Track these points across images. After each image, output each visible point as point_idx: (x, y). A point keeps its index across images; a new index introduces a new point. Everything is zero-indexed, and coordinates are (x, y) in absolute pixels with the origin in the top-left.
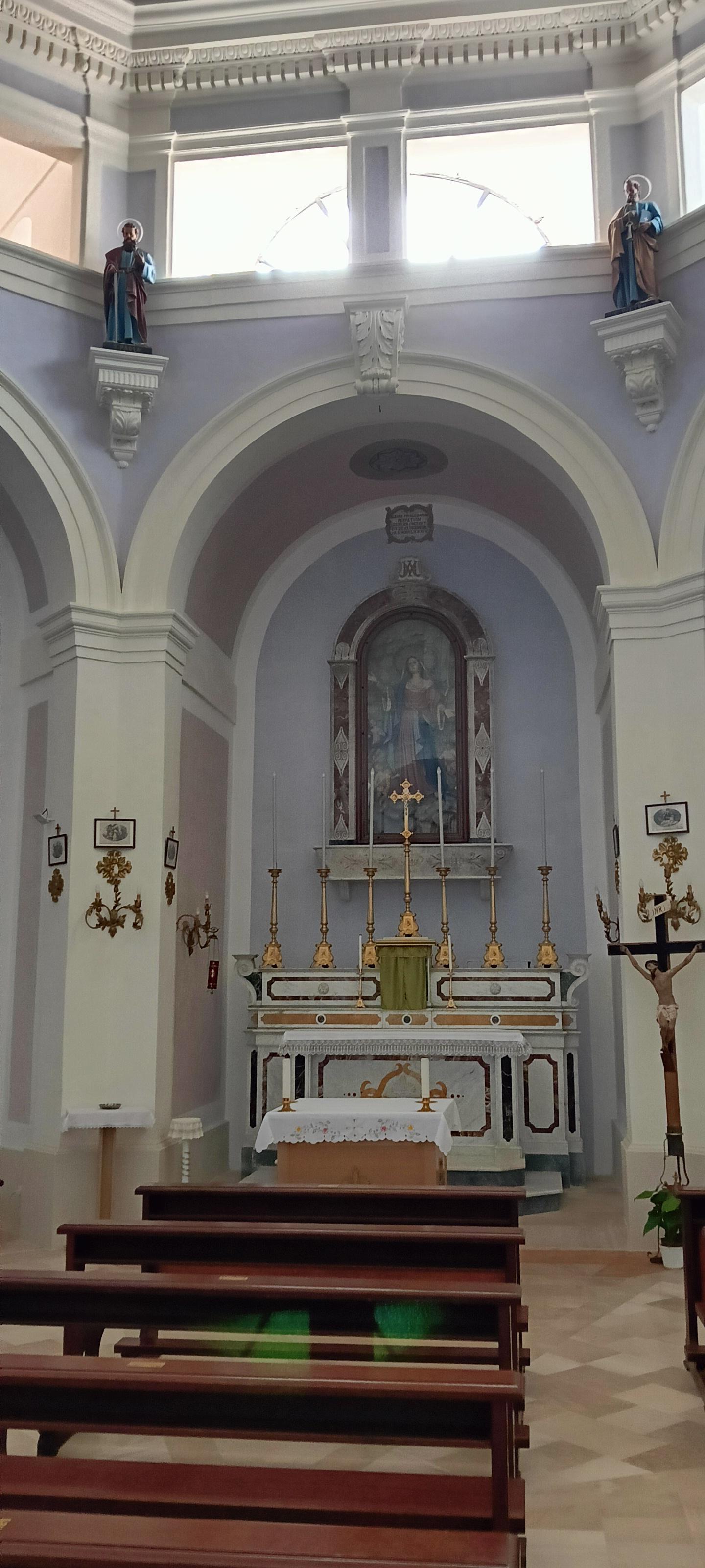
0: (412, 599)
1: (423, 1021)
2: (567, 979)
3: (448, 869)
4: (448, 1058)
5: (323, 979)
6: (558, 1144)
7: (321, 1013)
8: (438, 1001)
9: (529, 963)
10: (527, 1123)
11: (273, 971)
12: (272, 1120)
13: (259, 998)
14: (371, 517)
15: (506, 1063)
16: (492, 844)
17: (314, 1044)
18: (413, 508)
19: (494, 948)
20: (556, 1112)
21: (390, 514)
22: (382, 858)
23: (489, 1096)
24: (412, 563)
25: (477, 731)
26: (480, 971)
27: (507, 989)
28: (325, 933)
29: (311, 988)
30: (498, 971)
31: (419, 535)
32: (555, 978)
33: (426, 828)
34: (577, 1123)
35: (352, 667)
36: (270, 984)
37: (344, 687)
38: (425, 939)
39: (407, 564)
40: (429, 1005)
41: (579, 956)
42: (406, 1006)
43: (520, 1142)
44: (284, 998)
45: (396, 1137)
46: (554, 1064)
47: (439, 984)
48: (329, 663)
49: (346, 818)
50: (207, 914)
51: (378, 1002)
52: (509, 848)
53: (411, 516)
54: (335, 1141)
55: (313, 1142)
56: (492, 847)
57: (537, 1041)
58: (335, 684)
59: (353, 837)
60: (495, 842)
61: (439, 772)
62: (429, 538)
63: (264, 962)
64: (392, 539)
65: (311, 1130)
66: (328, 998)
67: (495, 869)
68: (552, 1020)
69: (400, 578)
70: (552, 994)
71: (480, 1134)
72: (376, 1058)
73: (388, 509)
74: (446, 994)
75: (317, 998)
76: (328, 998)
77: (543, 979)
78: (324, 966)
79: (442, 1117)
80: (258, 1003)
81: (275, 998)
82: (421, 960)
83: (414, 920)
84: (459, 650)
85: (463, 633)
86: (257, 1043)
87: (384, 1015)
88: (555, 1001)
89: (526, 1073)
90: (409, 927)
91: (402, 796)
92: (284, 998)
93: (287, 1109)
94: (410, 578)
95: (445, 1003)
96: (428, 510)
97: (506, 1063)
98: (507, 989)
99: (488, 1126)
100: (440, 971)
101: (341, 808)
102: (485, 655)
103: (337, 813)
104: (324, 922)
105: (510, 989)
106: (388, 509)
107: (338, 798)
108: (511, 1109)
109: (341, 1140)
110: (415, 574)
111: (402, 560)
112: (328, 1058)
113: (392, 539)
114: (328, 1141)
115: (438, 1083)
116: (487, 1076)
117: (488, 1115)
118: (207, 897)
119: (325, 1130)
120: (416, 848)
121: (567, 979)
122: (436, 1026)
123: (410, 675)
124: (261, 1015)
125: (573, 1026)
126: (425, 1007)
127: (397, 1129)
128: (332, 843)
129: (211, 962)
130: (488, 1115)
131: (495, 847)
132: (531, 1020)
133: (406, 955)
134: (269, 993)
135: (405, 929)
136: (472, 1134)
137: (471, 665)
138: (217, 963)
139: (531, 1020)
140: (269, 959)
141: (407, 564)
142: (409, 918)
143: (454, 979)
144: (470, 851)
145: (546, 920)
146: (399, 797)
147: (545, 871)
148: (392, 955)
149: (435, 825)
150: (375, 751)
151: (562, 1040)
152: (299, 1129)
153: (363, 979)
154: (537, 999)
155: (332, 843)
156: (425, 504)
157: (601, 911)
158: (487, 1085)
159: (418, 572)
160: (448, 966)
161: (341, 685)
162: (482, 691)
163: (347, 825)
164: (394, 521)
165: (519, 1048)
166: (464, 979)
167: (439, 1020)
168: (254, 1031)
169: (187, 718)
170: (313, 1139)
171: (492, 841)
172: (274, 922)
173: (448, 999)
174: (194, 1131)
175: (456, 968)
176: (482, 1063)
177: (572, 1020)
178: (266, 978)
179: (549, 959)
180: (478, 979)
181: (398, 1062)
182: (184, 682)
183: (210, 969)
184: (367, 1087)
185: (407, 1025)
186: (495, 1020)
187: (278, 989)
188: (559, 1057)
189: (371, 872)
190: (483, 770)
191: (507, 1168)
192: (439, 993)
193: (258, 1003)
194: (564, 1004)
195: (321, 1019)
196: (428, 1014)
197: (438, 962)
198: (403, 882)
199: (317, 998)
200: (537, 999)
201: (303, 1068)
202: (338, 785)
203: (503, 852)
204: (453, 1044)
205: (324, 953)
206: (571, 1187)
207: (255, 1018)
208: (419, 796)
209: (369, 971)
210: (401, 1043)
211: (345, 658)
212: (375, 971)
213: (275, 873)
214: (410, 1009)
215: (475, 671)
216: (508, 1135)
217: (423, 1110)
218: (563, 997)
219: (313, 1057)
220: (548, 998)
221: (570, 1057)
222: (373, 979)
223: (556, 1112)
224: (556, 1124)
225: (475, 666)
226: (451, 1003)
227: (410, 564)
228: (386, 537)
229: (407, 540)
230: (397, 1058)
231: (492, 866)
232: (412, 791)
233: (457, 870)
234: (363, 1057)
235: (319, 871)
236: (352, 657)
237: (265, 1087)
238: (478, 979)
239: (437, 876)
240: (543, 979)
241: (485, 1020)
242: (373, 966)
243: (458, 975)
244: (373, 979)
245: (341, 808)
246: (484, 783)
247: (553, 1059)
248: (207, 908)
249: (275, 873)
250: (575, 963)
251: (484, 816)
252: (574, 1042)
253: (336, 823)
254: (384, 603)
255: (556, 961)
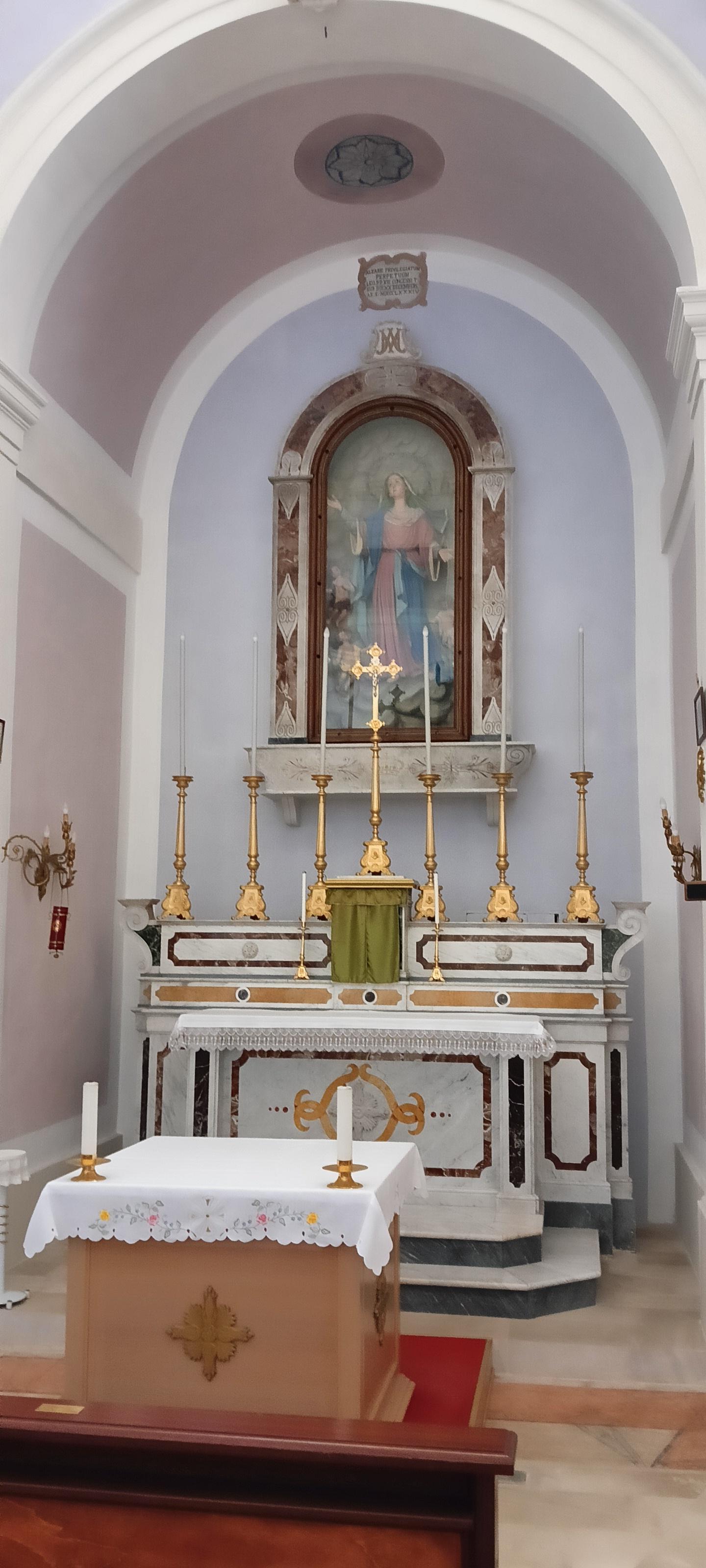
0: (397, 386)
1: (394, 999)
2: (612, 939)
3: (436, 778)
4: (427, 1058)
5: (249, 936)
6: (594, 1187)
7: (243, 986)
8: (417, 969)
9: (556, 916)
10: (549, 1155)
11: (177, 924)
12: (59, 1198)
13: (156, 962)
14: (334, 272)
15: (516, 1066)
16: (503, 743)
17: (224, 1034)
18: (398, 258)
19: (503, 892)
20: (593, 1138)
21: (365, 267)
22: (342, 763)
23: (489, 1116)
24: (394, 333)
25: (485, 578)
26: (481, 926)
27: (521, 953)
28: (254, 869)
29: (232, 949)
30: (509, 926)
31: (406, 297)
32: (595, 938)
33: (410, 723)
34: (625, 1155)
35: (305, 487)
36: (172, 942)
37: (293, 516)
38: (399, 878)
39: (387, 333)
40: (404, 975)
41: (632, 906)
42: (368, 976)
43: (538, 1186)
44: (191, 963)
45: (287, 1235)
46: (590, 1066)
47: (420, 945)
48: (272, 481)
49: (293, 706)
50: (66, 837)
51: (327, 971)
52: (530, 748)
53: (395, 270)
54: (171, 1239)
55: (131, 1241)
56: (503, 748)
57: (564, 1032)
58: (280, 512)
59: (302, 734)
60: (509, 739)
61: (425, 633)
62: (421, 301)
63: (165, 910)
64: (366, 305)
65: (128, 1217)
66: (257, 964)
67: (508, 777)
68: (590, 1001)
69: (376, 356)
70: (590, 961)
71: (474, 1174)
72: (319, 1055)
73: (362, 261)
74: (430, 960)
75: (240, 964)
76: (257, 964)
77: (575, 939)
78: (252, 918)
79: (373, 1201)
80: (155, 970)
81: (178, 963)
82: (392, 910)
83: (385, 851)
84: (462, 458)
85: (468, 434)
86: (149, 1028)
87: (336, 990)
88: (595, 972)
89: (547, 1079)
90: (376, 861)
91: (370, 669)
92: (191, 963)
93: (89, 1175)
94: (391, 355)
95: (426, 973)
96: (420, 263)
97: (516, 1066)
98: (521, 953)
99: (486, 1162)
100: (423, 926)
101: (285, 692)
102: (499, 465)
103: (280, 699)
104: (253, 853)
105: (526, 954)
106: (362, 261)
107: (283, 677)
108: (522, 1137)
109: (182, 1238)
110: (399, 350)
111: (381, 328)
112: (246, 1055)
113: (366, 305)
114: (158, 1238)
115: (411, 1095)
116: (487, 1084)
117: (487, 1144)
118: (66, 811)
119: (153, 1218)
120: (392, 752)
121: (612, 939)
122: (412, 1006)
123: (390, 500)
124: (155, 987)
125: (621, 1009)
126: (395, 978)
127: (287, 1219)
128: (272, 741)
129: (56, 908)
130: (487, 1144)
131: (508, 747)
132: (558, 1000)
133: (370, 902)
134: (171, 956)
135: (370, 864)
136: (462, 1173)
137: (479, 482)
138: (65, 910)
139: (558, 1000)
140: (171, 905)
141: (387, 334)
142: (376, 847)
143: (442, 938)
144: (471, 752)
145: (582, 852)
146: (365, 669)
147: (583, 778)
148: (350, 903)
149: (417, 713)
150: (340, 612)
151: (604, 1030)
152: (105, 1216)
153: (309, 937)
154: (566, 968)
155: (272, 741)
156: (416, 253)
157: (668, 834)
158: (487, 1098)
159: (402, 347)
160: (432, 919)
161: (289, 513)
162: (495, 520)
163: (295, 718)
164: (370, 278)
165: (535, 1046)
166: (458, 938)
167: (416, 998)
168: (144, 1010)
169: (32, 539)
170: (130, 1235)
171: (503, 738)
172: (180, 853)
173: (431, 966)
174: (12, 1173)
175: (446, 921)
176: (479, 1065)
177: (619, 1001)
178: (167, 934)
179: (586, 909)
180: (478, 938)
181: (352, 1061)
182: (19, 475)
183: (54, 919)
184: (304, 1098)
185: (370, 1005)
186: (502, 999)
187: (183, 950)
188: (598, 1056)
189: (324, 780)
190: (493, 635)
191: (512, 1235)
192: (420, 958)
193: (155, 970)
194: (608, 976)
195: (243, 995)
196: (400, 988)
197: (418, 912)
198: (368, 797)
199: (240, 964)
200: (566, 968)
201: (207, 1069)
202: (282, 659)
203: (519, 755)
204: (435, 1037)
205: (251, 899)
206: (614, 1250)
207: (148, 992)
208: (394, 669)
209: (316, 925)
210: (354, 1035)
211: (295, 473)
212: (326, 925)
213: (183, 781)
214: (374, 981)
215: (485, 488)
216: (517, 1177)
217: (338, 1184)
218: (607, 965)
219: (223, 1053)
220: (583, 968)
221: (615, 1057)
222: (323, 937)
223: (593, 1138)
224: (592, 1156)
225: (484, 482)
226: (437, 973)
227: (390, 334)
228: (359, 301)
229: (388, 305)
230: (350, 1055)
231: (502, 771)
232: (385, 661)
233: (451, 780)
234: (297, 1054)
235: (246, 779)
236: (306, 472)
237: (159, 1094)
238: (478, 938)
239: (419, 788)
240: (575, 939)
241: (486, 1000)
242: (322, 918)
243: (447, 931)
244: (583, 940)
245: (285, 692)
246: (494, 654)
247: (590, 1058)
248: (66, 828)
249: (183, 781)
250: (625, 915)
251: (493, 702)
252: (622, 1034)
253: (278, 712)
254: (352, 393)
255: (596, 912)
